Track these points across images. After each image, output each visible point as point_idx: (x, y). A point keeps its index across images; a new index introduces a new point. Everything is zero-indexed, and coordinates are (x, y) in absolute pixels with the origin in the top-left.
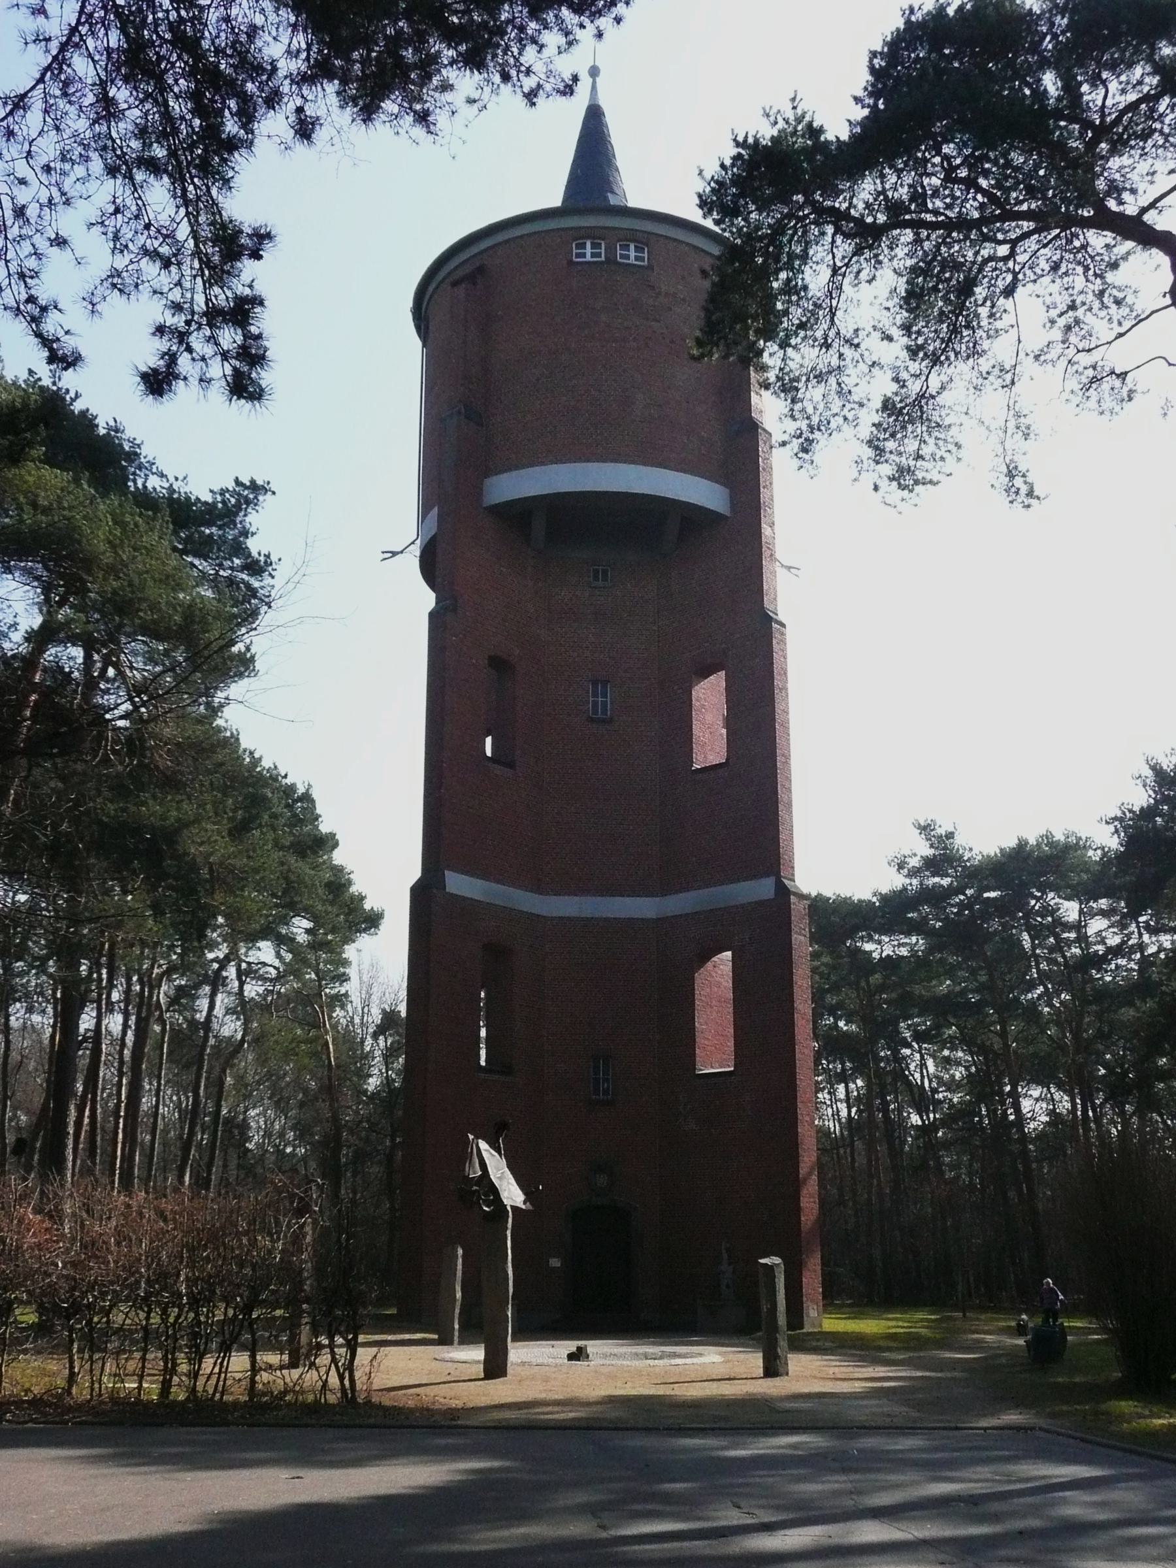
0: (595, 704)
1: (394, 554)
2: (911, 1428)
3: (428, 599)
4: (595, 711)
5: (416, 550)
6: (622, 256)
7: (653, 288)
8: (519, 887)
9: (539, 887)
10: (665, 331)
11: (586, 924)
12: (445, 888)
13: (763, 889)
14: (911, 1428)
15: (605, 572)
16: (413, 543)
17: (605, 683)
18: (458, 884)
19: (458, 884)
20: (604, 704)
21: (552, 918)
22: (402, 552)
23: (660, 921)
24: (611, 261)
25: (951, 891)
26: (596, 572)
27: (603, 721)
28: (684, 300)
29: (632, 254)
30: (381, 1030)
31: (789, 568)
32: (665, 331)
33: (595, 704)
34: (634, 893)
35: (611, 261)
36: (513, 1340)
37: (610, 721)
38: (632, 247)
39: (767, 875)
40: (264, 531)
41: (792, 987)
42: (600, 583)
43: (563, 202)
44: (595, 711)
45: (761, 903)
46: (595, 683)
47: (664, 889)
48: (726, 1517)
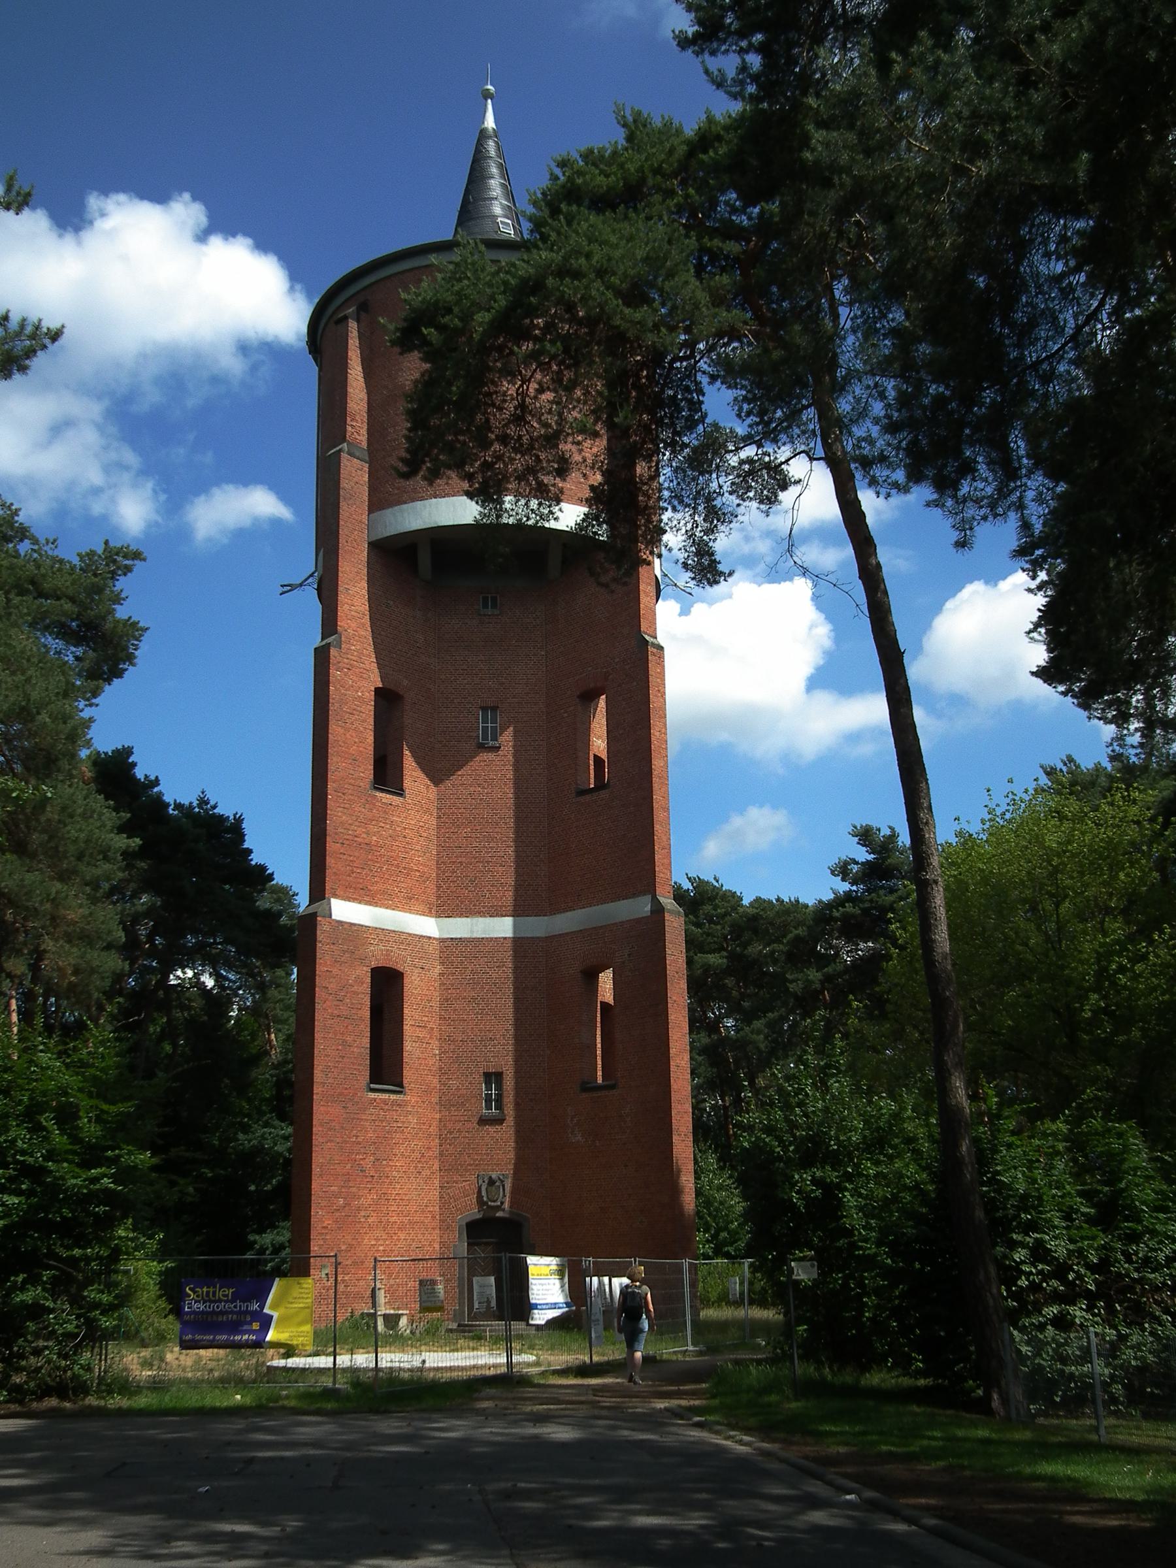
1: (293, 587)
4: (485, 737)
5: (313, 581)
8: (410, 911)
12: (330, 916)
13: (642, 907)
15: (494, 599)
16: (312, 575)
17: (494, 709)
22: (301, 585)
26: (485, 600)
33: (485, 729)
39: (643, 893)
41: (516, 1020)
42: (489, 611)
43: (340, 923)
44: (485, 737)
45: (639, 921)
48: (104, 1536)
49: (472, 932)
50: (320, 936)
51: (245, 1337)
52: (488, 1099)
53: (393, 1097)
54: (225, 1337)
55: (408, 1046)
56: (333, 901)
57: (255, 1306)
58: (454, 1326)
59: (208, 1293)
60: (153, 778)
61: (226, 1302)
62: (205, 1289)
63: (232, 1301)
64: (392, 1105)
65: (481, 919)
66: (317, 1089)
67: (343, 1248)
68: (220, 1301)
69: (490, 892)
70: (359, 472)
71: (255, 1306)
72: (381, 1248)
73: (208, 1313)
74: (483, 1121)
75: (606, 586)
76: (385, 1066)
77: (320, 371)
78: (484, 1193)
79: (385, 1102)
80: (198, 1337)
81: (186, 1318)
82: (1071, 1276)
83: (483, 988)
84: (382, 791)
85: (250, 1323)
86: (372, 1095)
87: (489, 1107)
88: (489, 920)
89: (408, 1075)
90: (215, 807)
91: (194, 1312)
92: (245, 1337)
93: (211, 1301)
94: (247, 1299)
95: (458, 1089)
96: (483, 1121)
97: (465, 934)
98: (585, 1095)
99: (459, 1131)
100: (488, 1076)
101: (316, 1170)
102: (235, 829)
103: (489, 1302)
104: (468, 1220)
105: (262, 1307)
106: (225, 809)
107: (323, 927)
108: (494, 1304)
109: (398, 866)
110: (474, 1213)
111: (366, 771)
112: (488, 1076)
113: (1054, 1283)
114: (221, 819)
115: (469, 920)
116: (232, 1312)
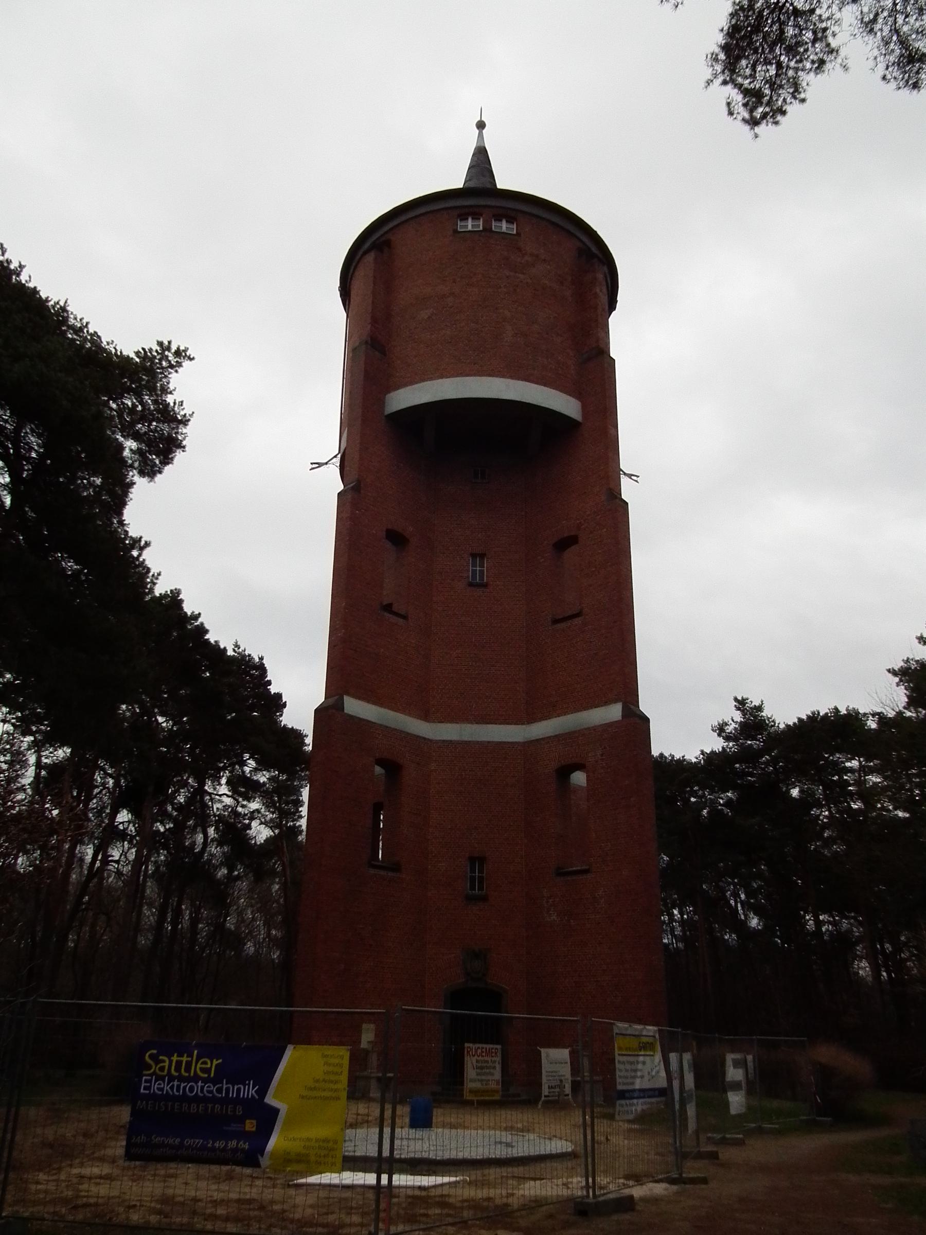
0: (474, 572)
1: (320, 465)
5: (337, 461)
7: (519, 249)
8: (410, 715)
9: (426, 716)
10: (529, 281)
11: (465, 746)
13: (614, 712)
16: (335, 457)
17: (482, 556)
18: (354, 706)
19: (354, 706)
20: (482, 572)
21: (437, 742)
22: (326, 463)
24: (487, 230)
25: (761, 752)
31: (630, 476)
32: (529, 281)
33: (474, 572)
34: (506, 722)
36: (741, 1081)
37: (486, 586)
40: (182, 388)
46: (474, 556)
47: (531, 718)
51: (233, 1144)
52: (473, 879)
53: (390, 874)
54: (199, 1142)
57: (250, 1091)
59: (179, 1064)
60: (197, 613)
61: (205, 1081)
62: (175, 1058)
63: (214, 1081)
68: (196, 1078)
71: (250, 1091)
73: (174, 1098)
74: (470, 899)
77: (347, 317)
80: (157, 1140)
86: (372, 871)
87: (473, 888)
88: (475, 727)
91: (153, 1097)
92: (233, 1144)
93: (181, 1079)
94: (237, 1078)
96: (470, 899)
100: (472, 860)
103: (561, 1086)
105: (263, 1092)
112: (472, 860)
115: (458, 725)
116: (214, 1100)
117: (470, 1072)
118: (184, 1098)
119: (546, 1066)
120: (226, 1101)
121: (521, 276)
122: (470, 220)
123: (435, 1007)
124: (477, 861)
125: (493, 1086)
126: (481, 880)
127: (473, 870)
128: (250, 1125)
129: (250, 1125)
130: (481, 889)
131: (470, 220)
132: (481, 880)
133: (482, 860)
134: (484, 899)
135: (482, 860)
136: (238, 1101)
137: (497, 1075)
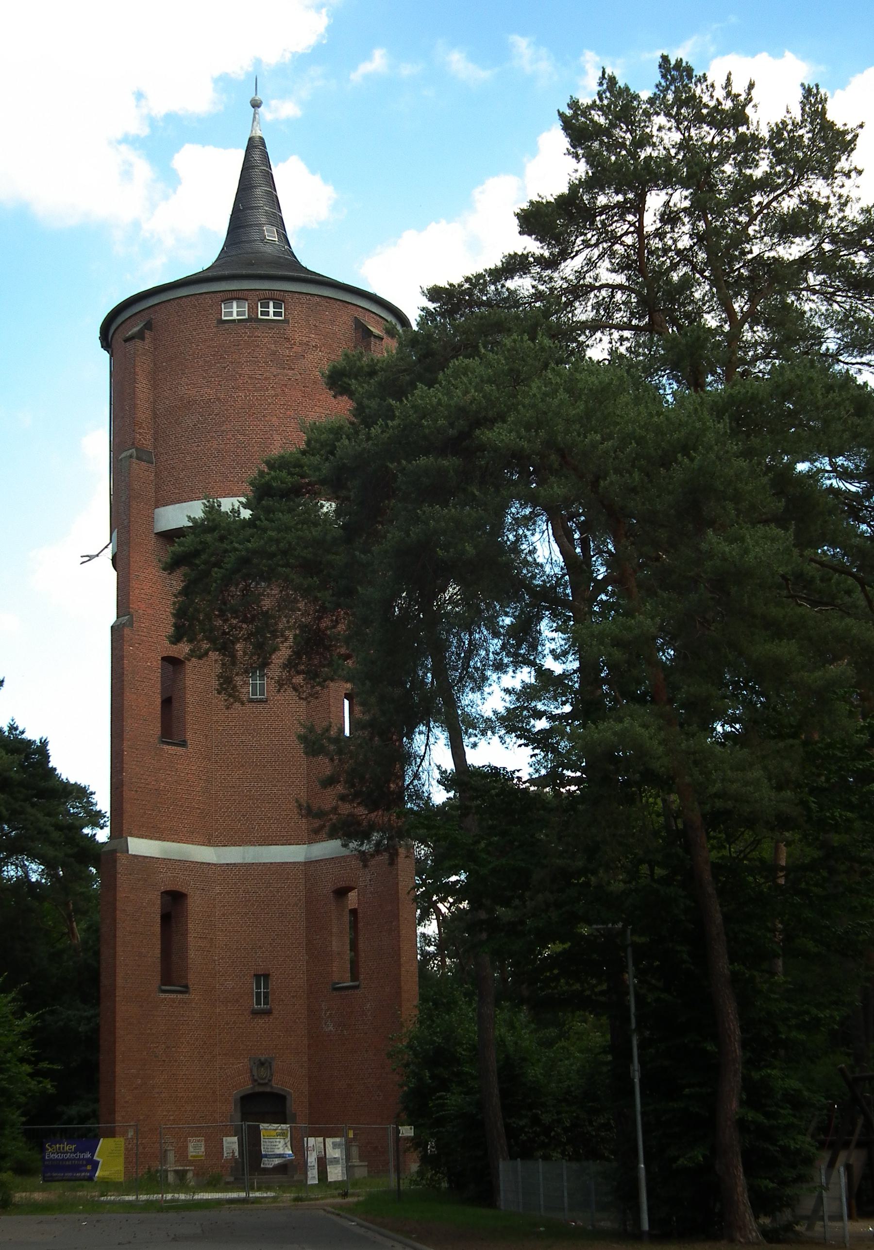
1: (91, 558)
2: (398, 1149)
3: (115, 573)
5: (109, 553)
6: (263, 313)
7: (287, 339)
10: (299, 377)
14: (398, 1149)
16: (106, 547)
22: (97, 555)
23: (308, 864)
27: (261, 701)
28: (316, 346)
29: (271, 310)
30: (757, 206)
32: (299, 377)
35: (253, 319)
38: (271, 304)
39: (477, 772)
43: (135, 856)
44: (254, 694)
49: (244, 858)
50: (120, 869)
53: (180, 996)
54: (70, 1174)
55: (192, 954)
56: (129, 838)
57: (88, 1155)
58: (231, 1179)
64: (179, 1003)
65: (252, 847)
66: (119, 993)
67: (141, 1118)
68: (67, 1152)
69: (259, 824)
70: (147, 473)
71: (88, 1155)
72: (172, 1118)
74: (255, 1013)
75: (305, 699)
76: (172, 973)
78: (255, 1073)
79: (173, 1001)
80: (54, 1174)
81: (46, 1163)
82: (553, 1134)
83: (253, 905)
84: (168, 743)
85: (86, 1166)
86: (163, 996)
87: (258, 1003)
89: (192, 979)
90: (23, 732)
94: (83, 1151)
95: (233, 988)
96: (255, 1013)
97: (239, 860)
98: (335, 993)
99: (234, 1022)
100: (257, 977)
101: (119, 1057)
102: (42, 750)
103: (233, 1152)
104: (242, 1094)
105: (93, 1156)
106: (32, 734)
107: (122, 860)
108: (237, 1154)
109: (182, 806)
110: (248, 1087)
111: (156, 728)
112: (257, 977)
113: (542, 1138)
114: (30, 743)
115: (241, 848)
116: (74, 1159)
117: (191, 1149)
118: (63, 1160)
119: (225, 1145)
120: (79, 1160)
121: (290, 372)
122: (235, 304)
123: (643, 1114)
124: (262, 978)
125: (201, 1154)
126: (266, 995)
127: (258, 987)
128: (89, 1167)
129: (89, 1167)
130: (266, 1003)
131: (235, 304)
132: (266, 995)
133: (266, 976)
134: (269, 1012)
135: (266, 976)
136: (83, 1159)
137: (203, 1149)
